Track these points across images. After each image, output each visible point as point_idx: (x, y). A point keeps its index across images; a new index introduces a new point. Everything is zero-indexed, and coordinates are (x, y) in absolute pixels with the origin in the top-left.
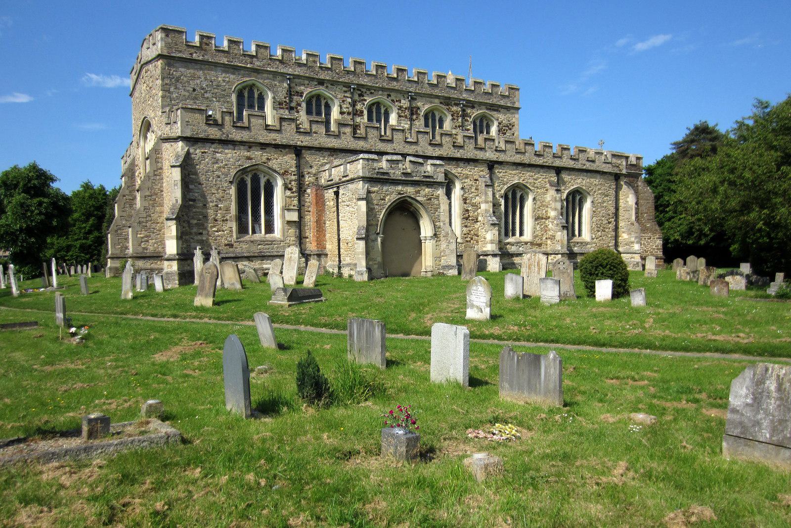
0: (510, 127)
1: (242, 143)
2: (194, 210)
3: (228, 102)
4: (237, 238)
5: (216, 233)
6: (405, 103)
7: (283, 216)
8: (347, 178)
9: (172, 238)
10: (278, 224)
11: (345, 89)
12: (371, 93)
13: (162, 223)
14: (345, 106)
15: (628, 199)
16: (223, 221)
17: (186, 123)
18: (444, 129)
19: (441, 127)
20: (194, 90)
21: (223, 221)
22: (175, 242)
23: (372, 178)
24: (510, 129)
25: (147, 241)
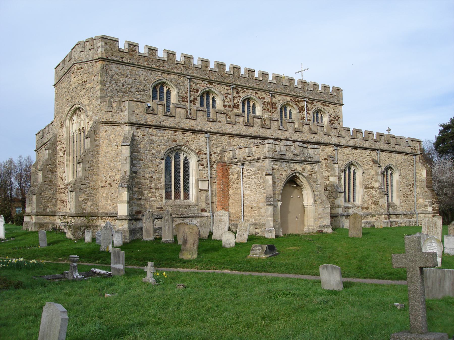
0: (337, 118)
1: (170, 128)
2: (136, 180)
3: (147, 95)
4: (165, 203)
5: (151, 199)
6: (267, 99)
7: (197, 186)
8: (253, 158)
9: (123, 202)
10: (193, 192)
11: (227, 88)
12: (245, 91)
13: (98, 189)
14: (227, 100)
15: (423, 173)
16: (156, 189)
17: (132, 112)
18: (217, 108)
19: (214, 107)
20: (123, 86)
21: (156, 189)
22: (126, 205)
23: (275, 158)
24: (337, 120)
25: (86, 203)
